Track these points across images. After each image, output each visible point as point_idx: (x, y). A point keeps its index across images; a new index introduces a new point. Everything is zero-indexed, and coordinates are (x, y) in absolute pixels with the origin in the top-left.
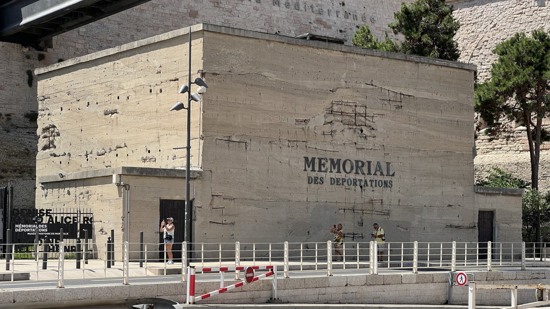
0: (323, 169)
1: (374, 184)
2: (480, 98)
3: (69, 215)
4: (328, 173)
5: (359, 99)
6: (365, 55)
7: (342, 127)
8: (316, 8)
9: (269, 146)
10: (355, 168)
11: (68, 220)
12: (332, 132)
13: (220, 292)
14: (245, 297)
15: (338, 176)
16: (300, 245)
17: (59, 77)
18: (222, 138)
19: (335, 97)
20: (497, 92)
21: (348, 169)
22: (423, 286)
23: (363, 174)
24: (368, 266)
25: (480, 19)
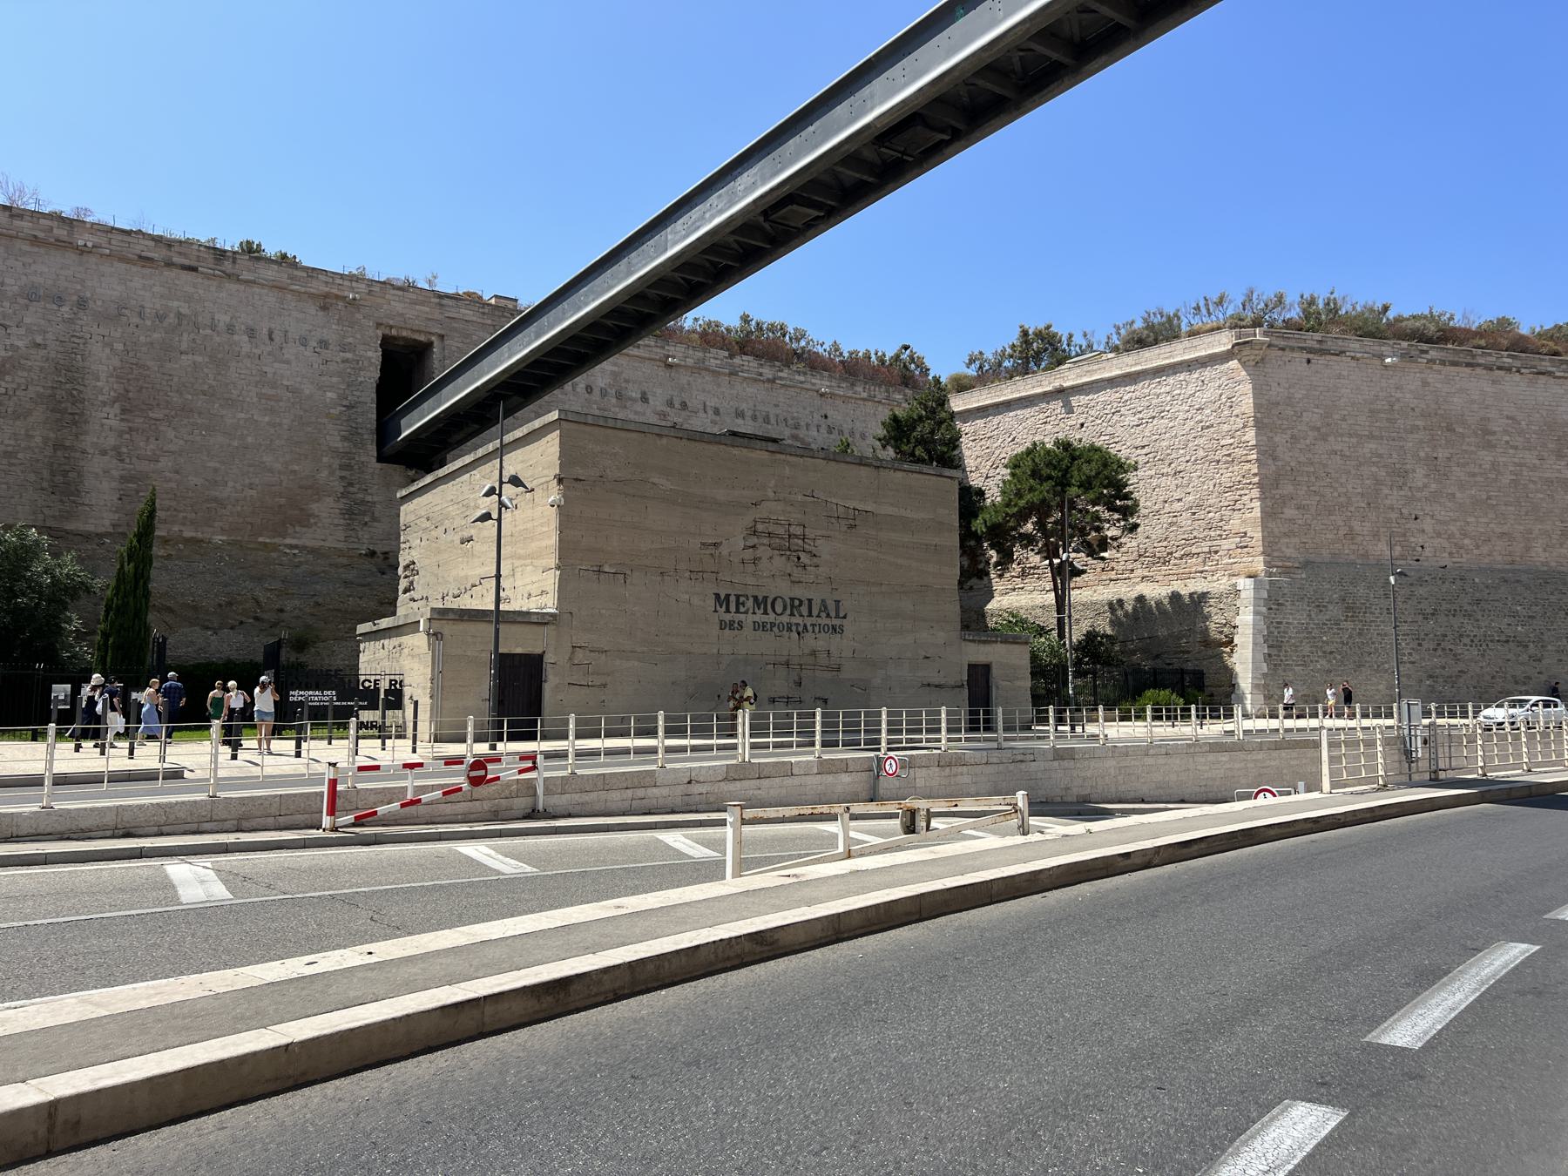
0: (742, 609)
1: (817, 629)
2: (985, 522)
3: (368, 677)
4: (750, 615)
5: (795, 516)
6: (802, 456)
7: (770, 552)
8: (790, 422)
9: (659, 578)
10: (789, 607)
11: (367, 684)
12: (755, 559)
13: (403, 806)
14: (480, 810)
15: (765, 618)
16: (686, 716)
17: (419, 499)
18: (589, 567)
19: (761, 512)
20: (1007, 514)
21: (779, 609)
22: (829, 778)
23: (801, 616)
24: (734, 747)
25: (995, 433)
